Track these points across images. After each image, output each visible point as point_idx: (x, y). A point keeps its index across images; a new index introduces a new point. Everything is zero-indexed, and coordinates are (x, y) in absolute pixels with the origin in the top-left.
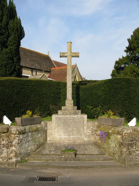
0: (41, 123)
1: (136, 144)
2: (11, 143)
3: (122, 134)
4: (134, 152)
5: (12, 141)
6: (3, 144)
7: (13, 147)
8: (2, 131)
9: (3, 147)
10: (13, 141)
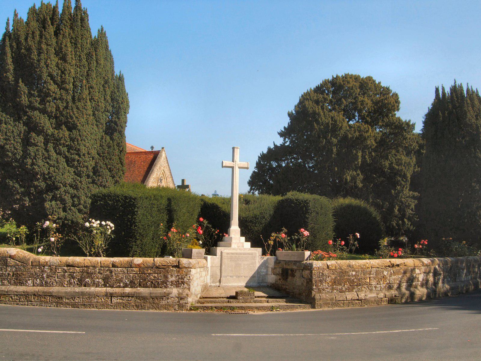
5: (183, 277)
6: (172, 282)
7: (185, 284)
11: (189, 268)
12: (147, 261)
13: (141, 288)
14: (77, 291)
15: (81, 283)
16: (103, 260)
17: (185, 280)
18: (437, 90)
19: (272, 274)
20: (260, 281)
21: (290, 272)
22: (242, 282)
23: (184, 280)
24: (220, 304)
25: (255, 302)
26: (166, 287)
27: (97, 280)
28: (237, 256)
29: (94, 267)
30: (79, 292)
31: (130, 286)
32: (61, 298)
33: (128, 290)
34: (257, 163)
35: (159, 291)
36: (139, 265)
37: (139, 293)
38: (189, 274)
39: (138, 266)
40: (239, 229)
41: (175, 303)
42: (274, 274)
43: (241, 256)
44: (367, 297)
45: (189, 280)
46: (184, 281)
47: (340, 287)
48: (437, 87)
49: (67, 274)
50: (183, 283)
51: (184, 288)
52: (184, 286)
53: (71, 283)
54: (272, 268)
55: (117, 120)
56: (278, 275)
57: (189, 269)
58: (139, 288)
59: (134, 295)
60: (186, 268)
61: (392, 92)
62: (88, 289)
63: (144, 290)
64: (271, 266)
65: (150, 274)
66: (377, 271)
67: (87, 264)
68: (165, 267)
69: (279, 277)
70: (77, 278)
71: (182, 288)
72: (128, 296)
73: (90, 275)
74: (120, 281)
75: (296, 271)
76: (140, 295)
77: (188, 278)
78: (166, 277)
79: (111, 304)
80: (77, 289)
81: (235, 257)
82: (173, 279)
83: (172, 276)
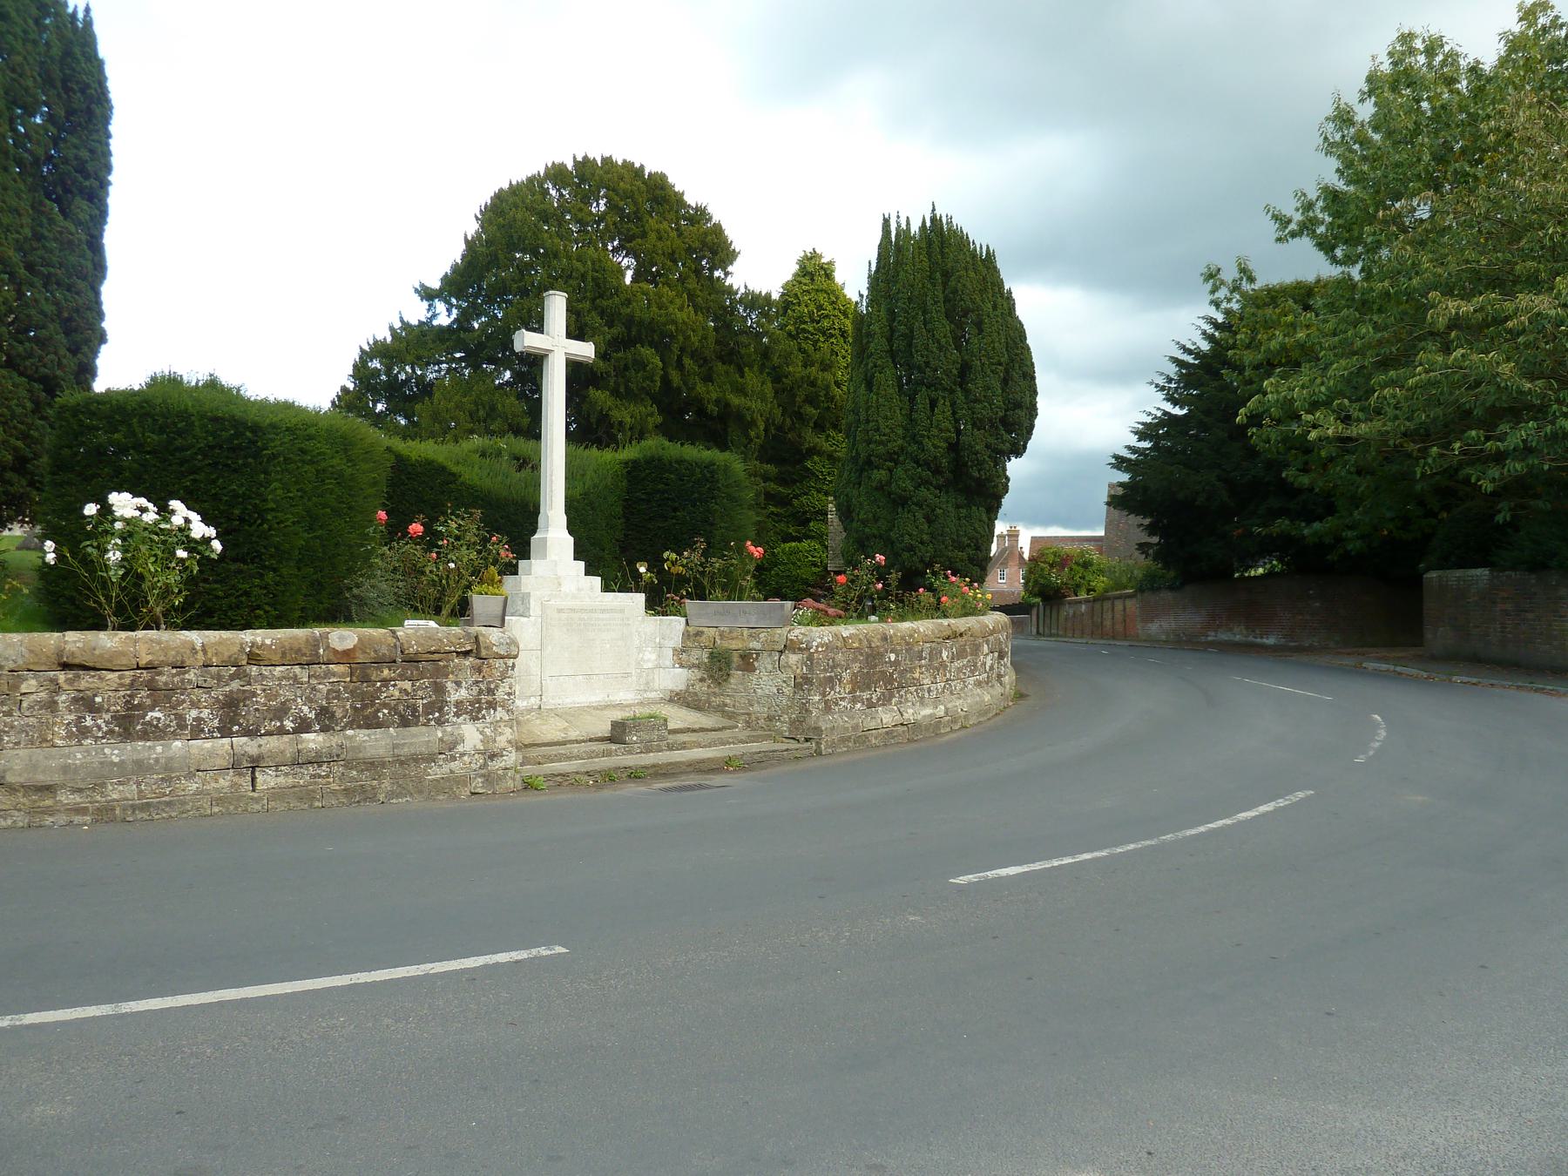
0: (502, 625)
1: (841, 677)
2: (488, 693)
3: (808, 648)
4: (837, 704)
5: (492, 686)
6: (458, 704)
7: (499, 709)
8: (453, 648)
9: (457, 715)
10: (497, 687)
11: (509, 657)
12: (371, 639)
13: (358, 730)
14: (116, 760)
15: (127, 725)
16: (213, 640)
17: (500, 695)
18: (886, 222)
19: (677, 665)
20: (642, 687)
21: (736, 659)
22: (597, 691)
23: (494, 695)
24: (583, 764)
25: (671, 748)
26: (440, 722)
27: (194, 713)
28: (585, 616)
29: (180, 667)
30: (122, 762)
31: (318, 727)
32: (48, 789)
33: (313, 740)
34: (355, 366)
35: (422, 737)
36: (347, 653)
37: (358, 749)
38: (509, 677)
39: (345, 656)
40: (571, 540)
41: (475, 770)
42: (682, 666)
43: (596, 615)
44: (919, 717)
45: (509, 694)
46: (495, 699)
47: (866, 695)
48: (887, 216)
49: (64, 697)
50: (492, 705)
51: (497, 722)
52: (497, 713)
53: (84, 732)
54: (675, 650)
55: (84, 154)
56: (698, 667)
57: (510, 662)
58: (349, 732)
59: (338, 756)
60: (502, 657)
61: (714, 221)
62: (159, 749)
63: (369, 735)
64: (672, 642)
65: (385, 682)
66: (932, 649)
67: (150, 658)
68: (436, 656)
69: (698, 674)
70: (108, 711)
71: (488, 720)
72: (316, 761)
73: (163, 696)
74: (281, 712)
75: (758, 655)
76: (361, 755)
77: (507, 690)
78: (440, 689)
79: (255, 795)
80: (115, 753)
81: (580, 619)
82: (463, 694)
83: (458, 684)
